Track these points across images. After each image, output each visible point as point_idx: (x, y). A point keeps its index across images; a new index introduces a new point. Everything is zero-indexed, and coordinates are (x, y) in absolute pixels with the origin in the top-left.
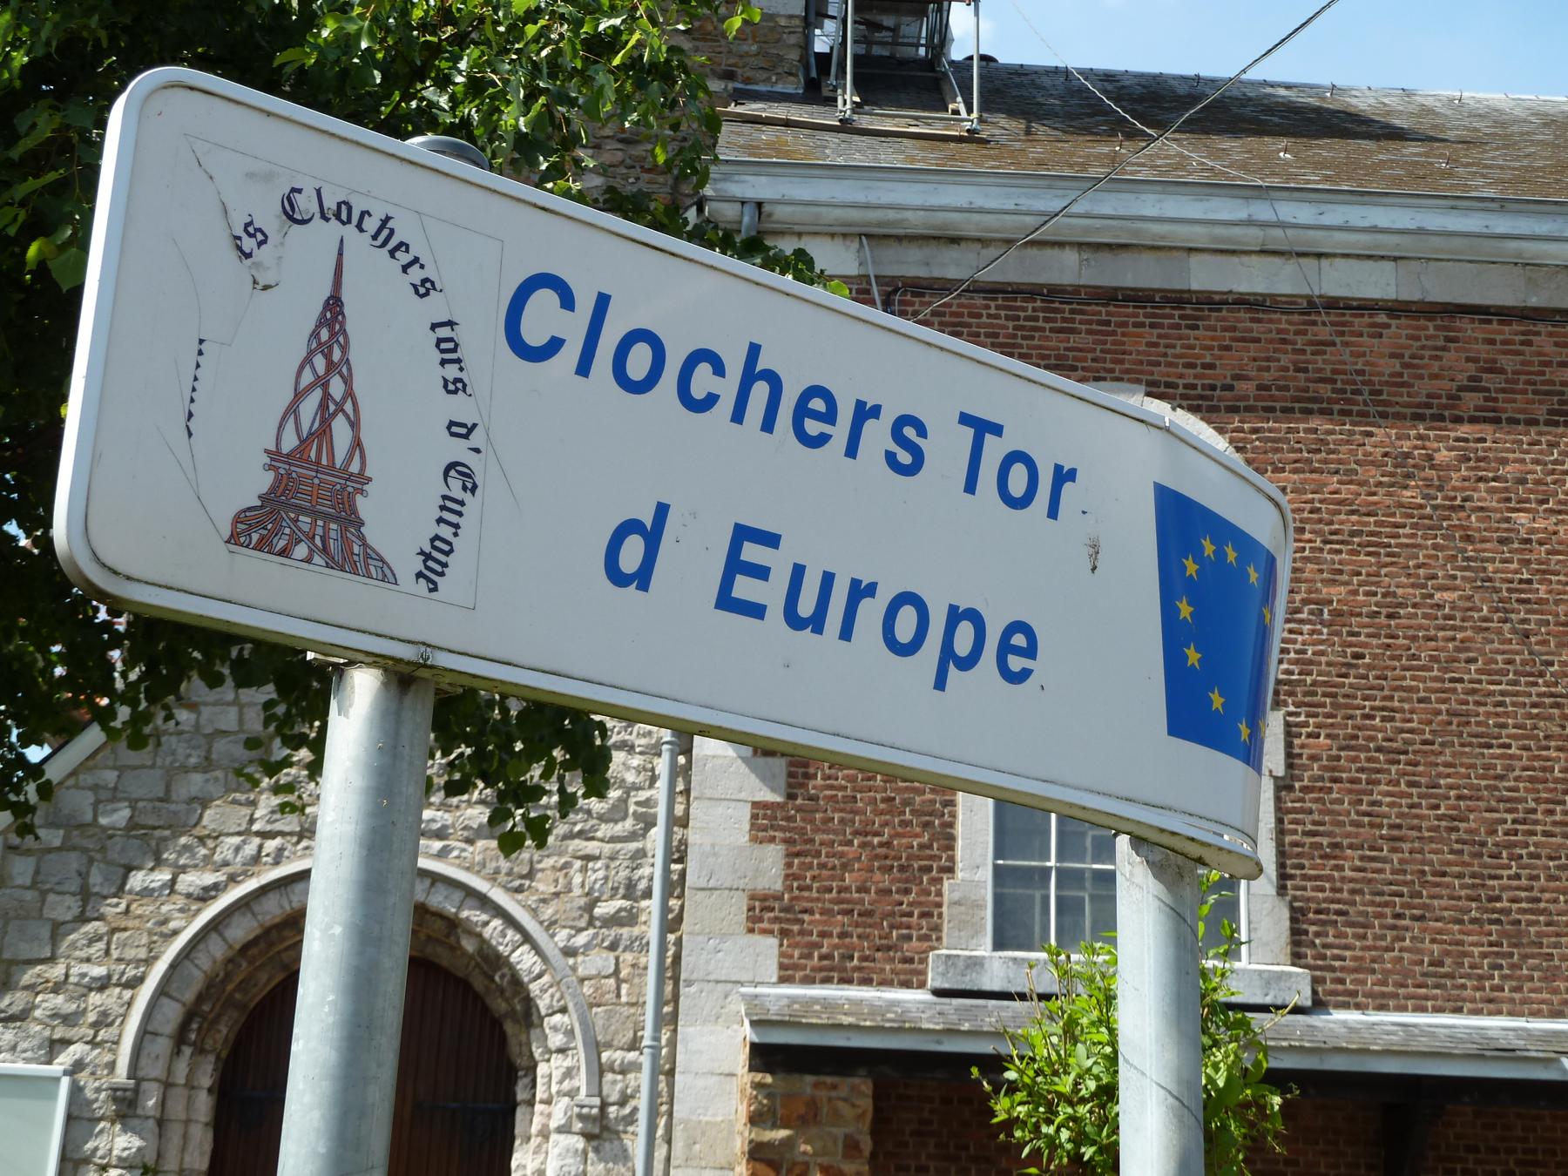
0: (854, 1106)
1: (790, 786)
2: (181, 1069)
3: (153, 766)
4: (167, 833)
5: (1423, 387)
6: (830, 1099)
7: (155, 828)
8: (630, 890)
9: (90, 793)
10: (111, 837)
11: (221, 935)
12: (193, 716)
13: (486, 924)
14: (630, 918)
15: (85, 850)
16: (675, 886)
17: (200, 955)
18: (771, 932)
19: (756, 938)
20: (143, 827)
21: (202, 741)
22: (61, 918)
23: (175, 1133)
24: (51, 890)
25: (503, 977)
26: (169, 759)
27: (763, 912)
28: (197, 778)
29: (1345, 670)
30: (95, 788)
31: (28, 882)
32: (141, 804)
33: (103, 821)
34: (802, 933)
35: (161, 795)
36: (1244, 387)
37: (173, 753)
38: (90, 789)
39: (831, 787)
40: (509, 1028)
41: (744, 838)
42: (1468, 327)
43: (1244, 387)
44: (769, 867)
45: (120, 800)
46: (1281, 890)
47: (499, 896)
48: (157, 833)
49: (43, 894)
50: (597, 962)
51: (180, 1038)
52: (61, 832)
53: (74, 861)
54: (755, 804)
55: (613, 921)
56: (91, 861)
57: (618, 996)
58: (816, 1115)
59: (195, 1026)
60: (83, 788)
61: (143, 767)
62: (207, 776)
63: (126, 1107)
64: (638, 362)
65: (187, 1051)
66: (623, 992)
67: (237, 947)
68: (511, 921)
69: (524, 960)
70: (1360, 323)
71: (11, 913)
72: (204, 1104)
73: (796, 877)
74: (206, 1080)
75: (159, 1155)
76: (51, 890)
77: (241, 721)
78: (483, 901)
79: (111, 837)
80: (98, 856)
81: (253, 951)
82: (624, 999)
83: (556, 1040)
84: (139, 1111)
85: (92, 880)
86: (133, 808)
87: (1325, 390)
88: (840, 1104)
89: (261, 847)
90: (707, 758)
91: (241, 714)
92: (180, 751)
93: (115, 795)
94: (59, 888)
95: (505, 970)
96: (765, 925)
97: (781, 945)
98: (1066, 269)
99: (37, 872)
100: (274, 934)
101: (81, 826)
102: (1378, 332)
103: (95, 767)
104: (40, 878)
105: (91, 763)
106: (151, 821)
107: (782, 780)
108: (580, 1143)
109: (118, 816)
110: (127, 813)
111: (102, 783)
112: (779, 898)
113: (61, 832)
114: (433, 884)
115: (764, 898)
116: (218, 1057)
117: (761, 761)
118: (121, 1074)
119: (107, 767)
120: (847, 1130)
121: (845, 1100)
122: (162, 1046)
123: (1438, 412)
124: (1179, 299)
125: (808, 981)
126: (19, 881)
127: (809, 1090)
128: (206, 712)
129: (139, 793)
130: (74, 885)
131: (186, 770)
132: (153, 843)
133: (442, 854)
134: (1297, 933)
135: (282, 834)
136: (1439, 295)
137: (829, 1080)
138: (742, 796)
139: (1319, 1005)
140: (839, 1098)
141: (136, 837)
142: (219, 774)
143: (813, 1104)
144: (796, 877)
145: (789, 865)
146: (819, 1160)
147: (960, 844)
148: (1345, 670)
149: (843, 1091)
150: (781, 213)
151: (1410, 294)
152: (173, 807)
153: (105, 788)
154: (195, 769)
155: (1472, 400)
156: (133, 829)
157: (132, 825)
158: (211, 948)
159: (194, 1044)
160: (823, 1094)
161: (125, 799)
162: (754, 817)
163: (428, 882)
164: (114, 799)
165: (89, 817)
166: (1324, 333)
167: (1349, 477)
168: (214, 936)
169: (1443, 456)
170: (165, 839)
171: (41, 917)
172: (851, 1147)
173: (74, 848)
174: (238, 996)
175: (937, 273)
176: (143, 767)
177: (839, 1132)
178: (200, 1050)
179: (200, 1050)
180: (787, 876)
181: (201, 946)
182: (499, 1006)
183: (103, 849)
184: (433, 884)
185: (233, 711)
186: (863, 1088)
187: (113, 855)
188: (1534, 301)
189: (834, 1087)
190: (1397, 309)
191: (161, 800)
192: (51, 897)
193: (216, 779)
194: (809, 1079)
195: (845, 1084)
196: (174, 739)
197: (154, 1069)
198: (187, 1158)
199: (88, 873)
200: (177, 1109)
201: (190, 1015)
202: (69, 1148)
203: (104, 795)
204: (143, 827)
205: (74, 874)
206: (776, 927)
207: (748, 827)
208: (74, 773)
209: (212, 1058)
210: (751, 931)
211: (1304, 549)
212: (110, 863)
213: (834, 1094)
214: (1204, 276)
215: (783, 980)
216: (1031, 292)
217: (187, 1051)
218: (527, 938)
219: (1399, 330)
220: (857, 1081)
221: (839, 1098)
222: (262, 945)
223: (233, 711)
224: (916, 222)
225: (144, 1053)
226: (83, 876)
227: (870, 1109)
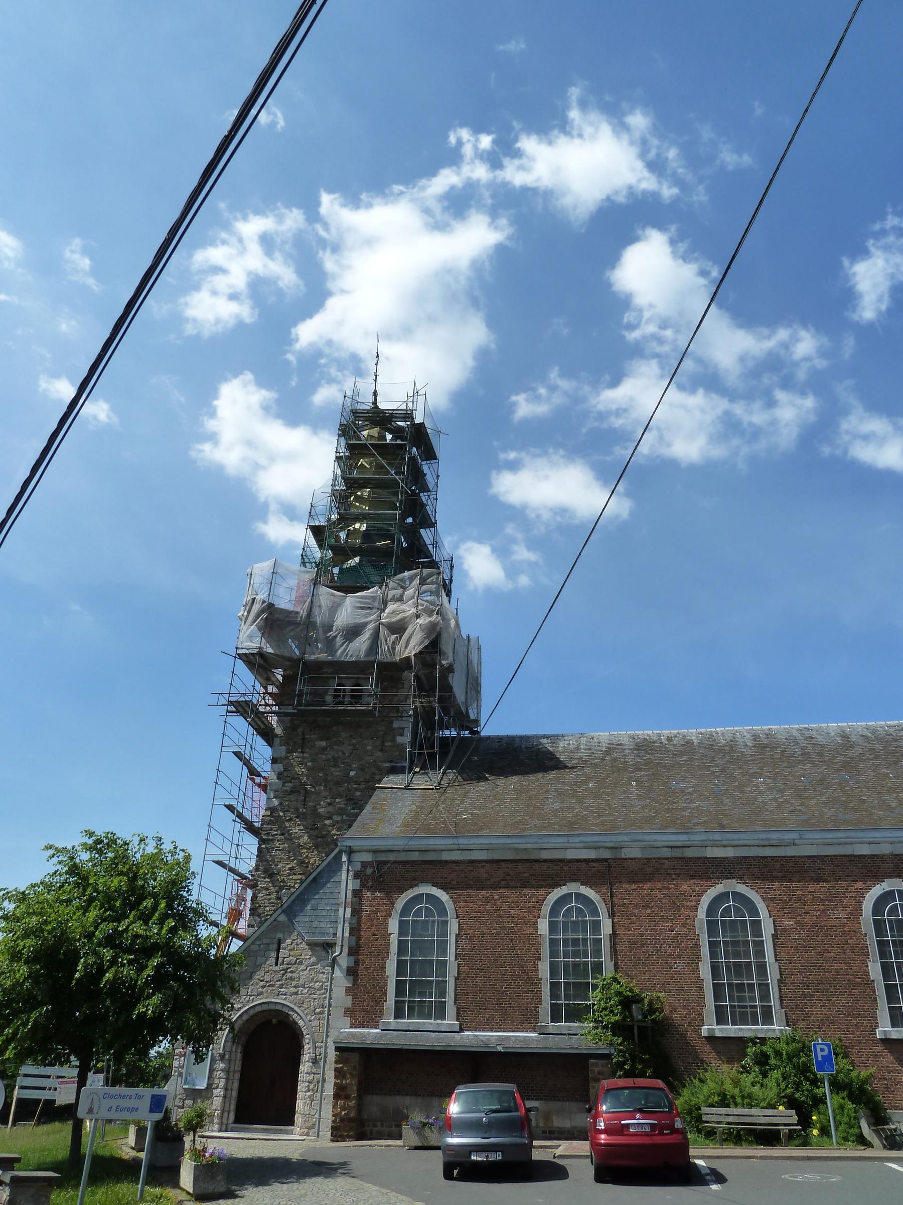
5: (492, 880)
8: (323, 1006)
14: (323, 1013)
16: (330, 1005)
23: (233, 1062)
27: (348, 1012)
29: (471, 950)
36: (454, 883)
42: (503, 865)
43: (454, 883)
44: (348, 1002)
46: (455, 1003)
47: (296, 1008)
50: (316, 1023)
55: (319, 1013)
63: (222, 1057)
64: (112, 1097)
68: (298, 1014)
69: (301, 1023)
70: (479, 865)
72: (239, 1056)
78: (293, 1010)
83: (307, 1041)
87: (471, 882)
98: (415, 856)
102: (483, 867)
108: (311, 1064)
118: (221, 1052)
122: (229, 1044)
123: (495, 887)
124: (440, 862)
125: (356, 1028)
133: (285, 999)
134: (458, 1014)
136: (496, 858)
139: (462, 1030)
147: (722, 730)
148: (471, 950)
150: (355, 848)
151: (490, 858)
155: (503, 883)
166: (471, 868)
167: (475, 903)
169: (496, 897)
172: (355, 1068)
175: (388, 859)
178: (238, 1044)
179: (238, 1044)
188: (518, 858)
190: (487, 861)
197: (228, 1049)
200: (233, 1057)
214: (445, 856)
215: (220, 1131)
216: (407, 862)
219: (488, 867)
224: (383, 848)
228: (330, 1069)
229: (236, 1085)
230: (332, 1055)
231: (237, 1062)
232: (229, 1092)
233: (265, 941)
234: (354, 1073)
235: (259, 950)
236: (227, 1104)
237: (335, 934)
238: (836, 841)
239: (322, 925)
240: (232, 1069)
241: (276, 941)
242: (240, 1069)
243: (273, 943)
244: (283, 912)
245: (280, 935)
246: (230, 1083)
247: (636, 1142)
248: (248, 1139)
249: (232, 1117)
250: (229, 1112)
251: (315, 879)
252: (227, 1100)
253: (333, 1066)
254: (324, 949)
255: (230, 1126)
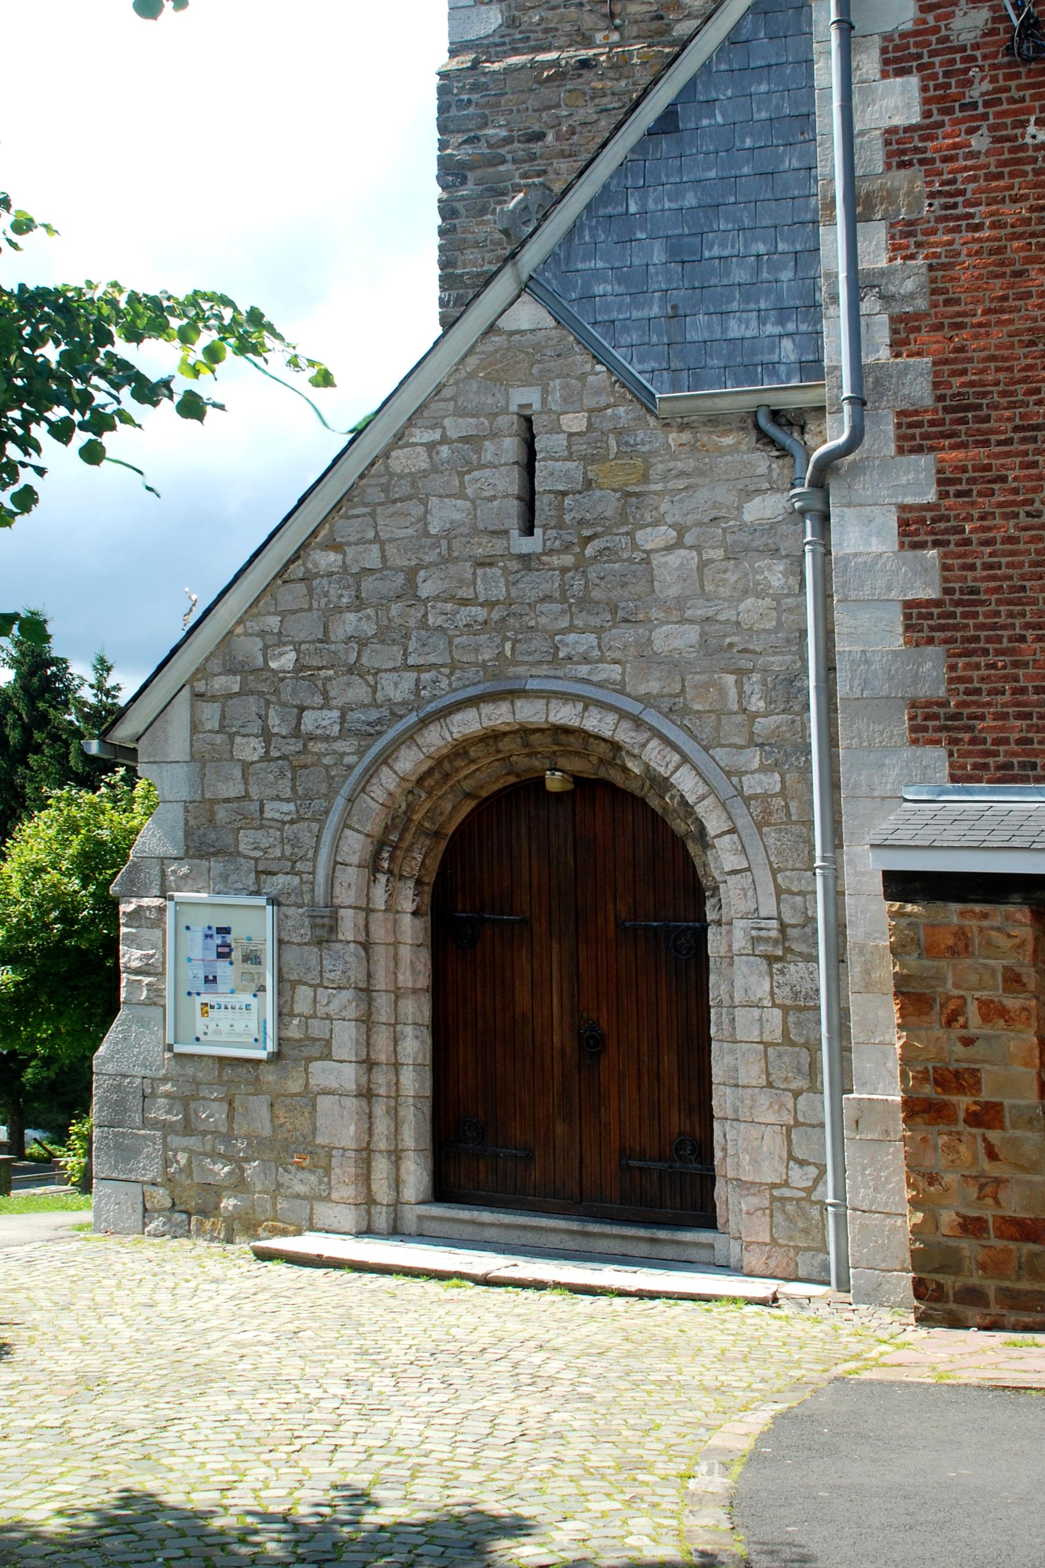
0: (1010, 936)
1: (946, 580)
2: (379, 896)
3: (310, 609)
4: (331, 672)
6: (981, 929)
7: (320, 669)
9: (258, 639)
10: (282, 680)
11: (391, 768)
12: (340, 557)
13: (644, 746)
15: (261, 694)
17: (374, 788)
18: (938, 742)
19: (919, 751)
20: (309, 668)
21: (351, 580)
22: (249, 759)
24: (237, 733)
25: (672, 798)
26: (323, 601)
27: (929, 722)
28: (351, 617)
30: (262, 634)
31: (217, 728)
32: (304, 647)
33: (273, 665)
34: (973, 741)
35: (320, 636)
37: (326, 594)
38: (257, 635)
39: (994, 578)
40: (692, 848)
41: (898, 642)
44: (931, 673)
45: (285, 644)
48: (322, 673)
49: (231, 736)
51: (373, 866)
52: (238, 678)
53: (253, 705)
54: (908, 605)
56: (268, 703)
57: (788, 814)
58: (967, 946)
59: (386, 855)
60: (251, 635)
61: (301, 610)
62: (360, 615)
65: (382, 878)
66: (793, 810)
67: (414, 778)
69: (686, 783)
71: (207, 756)
73: (960, 680)
74: (407, 904)
75: (369, 976)
76: (237, 733)
77: (384, 558)
79: (282, 680)
80: (274, 699)
81: (429, 782)
82: (794, 818)
84: (341, 937)
85: (270, 722)
86: (298, 651)
88: (993, 933)
89: (418, 680)
90: (846, 558)
91: (383, 551)
92: (332, 592)
93: (280, 639)
94: (243, 731)
95: (674, 792)
96: (930, 735)
97: (951, 754)
99: (223, 717)
100: (446, 764)
101: (254, 671)
103: (259, 614)
104: (227, 722)
105: (255, 610)
106: (316, 662)
107: (936, 575)
109: (285, 660)
110: (293, 655)
111: (267, 629)
112: (945, 704)
113: (238, 678)
114: (585, 708)
115: (929, 704)
116: (419, 882)
117: (910, 554)
119: (269, 613)
120: (1005, 962)
121: (999, 929)
126: (209, 726)
127: (955, 920)
128: (350, 551)
129: (302, 636)
130: (255, 728)
131: (339, 610)
132: (319, 683)
135: (432, 666)
137: (977, 908)
138: (893, 595)
140: (993, 928)
141: (303, 678)
142: (370, 611)
143: (961, 933)
144: (960, 680)
145: (952, 668)
146: (977, 994)
149: (997, 921)
152: (333, 647)
153: (271, 633)
154: (348, 608)
156: (301, 671)
157: (299, 667)
158: (384, 781)
159: (390, 872)
160: (973, 924)
161: (290, 643)
162: (908, 617)
163: (580, 706)
164: (280, 644)
165: (260, 662)
168: (385, 769)
170: (330, 679)
171: (232, 759)
172: (1013, 980)
173: (252, 693)
174: (426, 824)
176: (301, 610)
177: (997, 964)
180: (951, 680)
181: (374, 780)
182: (680, 827)
183: (276, 692)
184: (585, 708)
185: (375, 548)
186: (1019, 916)
187: (286, 696)
189: (985, 916)
191: (321, 641)
192: (238, 739)
193: (368, 617)
194: (955, 907)
195: (998, 913)
196: (325, 581)
198: (401, 978)
199: (267, 716)
201: (381, 844)
202: (285, 970)
203: (271, 640)
204: (309, 668)
205: (256, 718)
206: (943, 735)
207: (900, 629)
208: (241, 621)
209: (411, 884)
210: (915, 742)
211: (953, 62)
212: (284, 705)
213: (985, 923)
215: (367, 1231)
217: (382, 878)
218: (685, 759)
220: (1011, 908)
221: (993, 928)
222: (437, 776)
223: (375, 548)
225: (337, 883)
226: (263, 718)
227: (1030, 939)
228: (868, 987)
229: (415, 1047)
230: (872, 918)
231: (405, 953)
232: (381, 1080)
233: (454, 427)
234: (1013, 1003)
235: (435, 469)
236: (382, 1126)
237: (812, 368)
238: (976, 844)
239: (735, 330)
240: (381, 982)
241: (508, 422)
242: (424, 981)
243: (495, 435)
244: (528, 286)
245: (527, 396)
246: (382, 1041)
247: (537, 1219)
248: (641, 1295)
249: (416, 1176)
250: (396, 1155)
251: (668, 122)
252: (380, 1109)
253: (887, 969)
254: (765, 439)
255: (411, 1214)
